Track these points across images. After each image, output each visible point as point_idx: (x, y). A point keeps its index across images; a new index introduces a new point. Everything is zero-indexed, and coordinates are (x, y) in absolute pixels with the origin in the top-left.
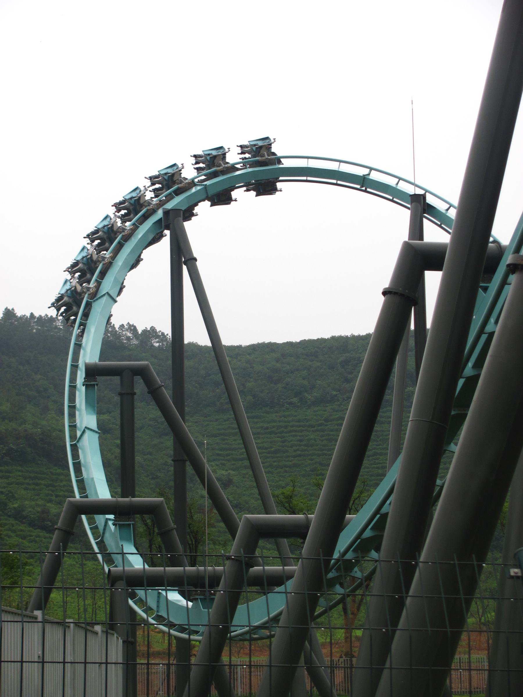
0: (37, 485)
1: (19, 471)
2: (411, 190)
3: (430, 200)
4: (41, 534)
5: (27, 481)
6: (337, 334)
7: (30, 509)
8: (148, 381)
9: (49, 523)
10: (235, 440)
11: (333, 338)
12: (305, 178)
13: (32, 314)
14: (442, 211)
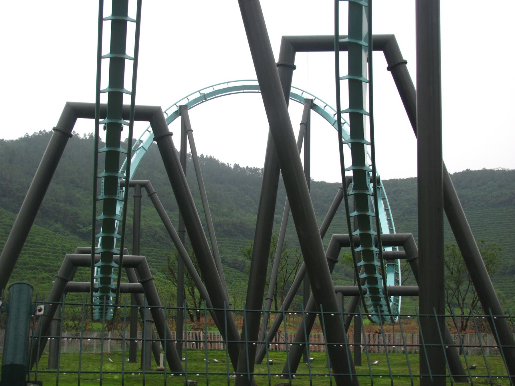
0: (236, 247)
1: (228, 240)
2: (305, 96)
3: (316, 102)
4: (233, 270)
5: (231, 245)
6: (392, 178)
7: (229, 258)
8: (148, 190)
9: (237, 265)
10: (339, 228)
11: (391, 180)
12: (242, 91)
13: (247, 167)
14: (321, 108)
